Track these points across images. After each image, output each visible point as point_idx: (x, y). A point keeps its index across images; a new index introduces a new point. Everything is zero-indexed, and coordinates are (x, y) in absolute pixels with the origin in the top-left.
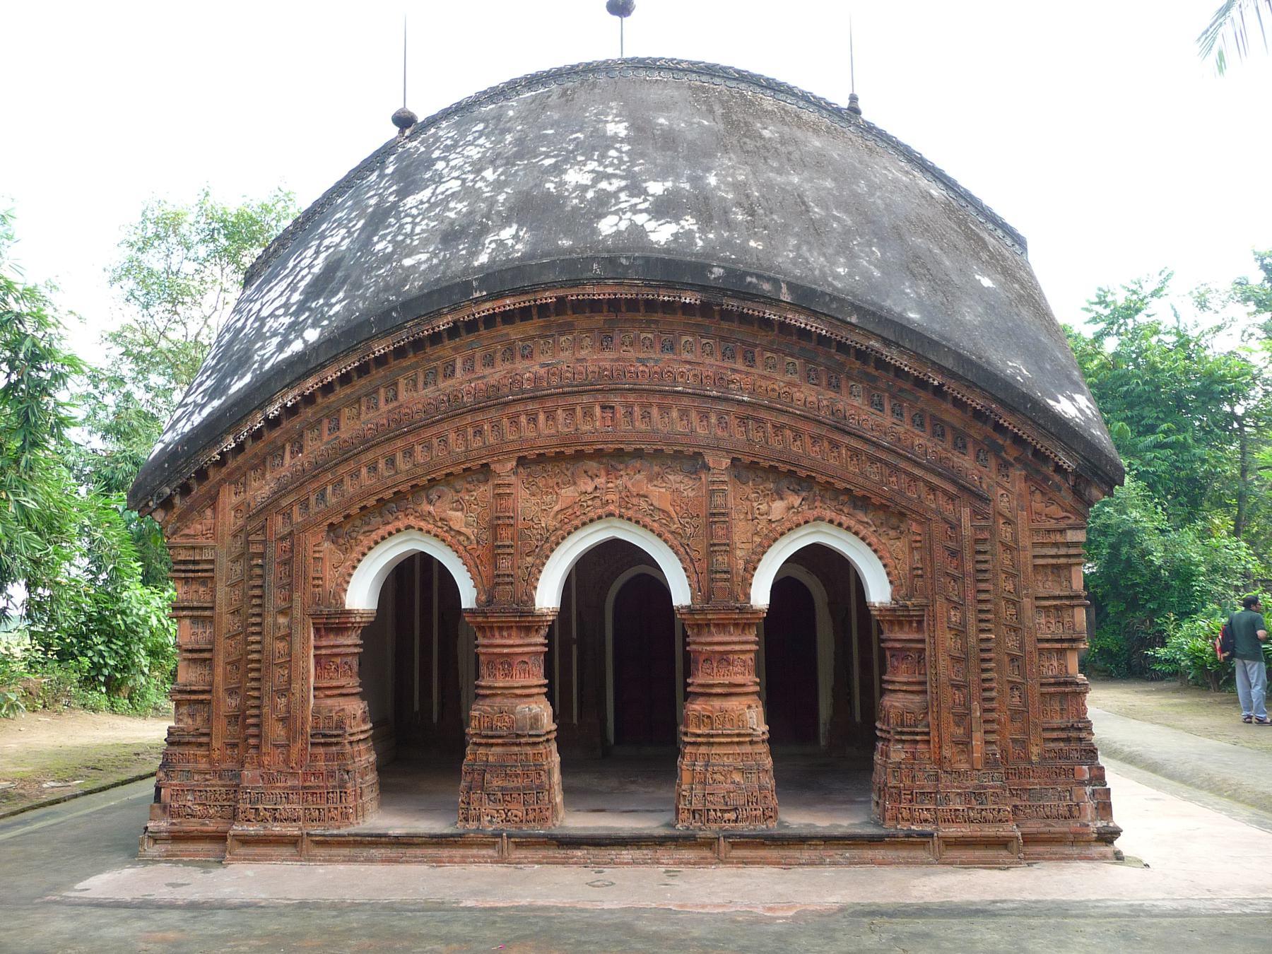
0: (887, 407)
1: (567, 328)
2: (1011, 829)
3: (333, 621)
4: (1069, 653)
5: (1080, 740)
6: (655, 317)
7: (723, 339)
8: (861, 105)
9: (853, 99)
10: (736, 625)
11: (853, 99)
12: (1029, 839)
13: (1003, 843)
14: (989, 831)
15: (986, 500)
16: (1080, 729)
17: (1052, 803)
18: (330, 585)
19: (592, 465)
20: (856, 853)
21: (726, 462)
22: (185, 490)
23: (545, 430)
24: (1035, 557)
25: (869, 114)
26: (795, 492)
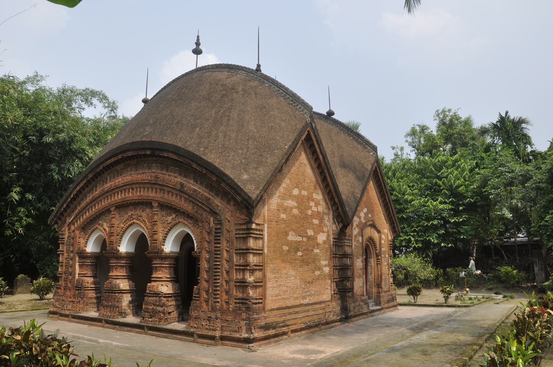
0: (199, 182)
1: (129, 165)
2: (218, 334)
3: (82, 255)
4: (246, 271)
5: (246, 303)
6: (146, 159)
7: (161, 164)
8: (262, 68)
9: (259, 66)
10: (159, 258)
11: (259, 66)
12: (223, 338)
13: (213, 338)
14: (210, 333)
15: (218, 214)
16: (246, 300)
17: (234, 327)
18: (82, 245)
19: (131, 207)
20: (129, 329)
21: (157, 204)
22: (60, 219)
23: (119, 197)
24: (236, 234)
25: (265, 71)
26: (175, 213)
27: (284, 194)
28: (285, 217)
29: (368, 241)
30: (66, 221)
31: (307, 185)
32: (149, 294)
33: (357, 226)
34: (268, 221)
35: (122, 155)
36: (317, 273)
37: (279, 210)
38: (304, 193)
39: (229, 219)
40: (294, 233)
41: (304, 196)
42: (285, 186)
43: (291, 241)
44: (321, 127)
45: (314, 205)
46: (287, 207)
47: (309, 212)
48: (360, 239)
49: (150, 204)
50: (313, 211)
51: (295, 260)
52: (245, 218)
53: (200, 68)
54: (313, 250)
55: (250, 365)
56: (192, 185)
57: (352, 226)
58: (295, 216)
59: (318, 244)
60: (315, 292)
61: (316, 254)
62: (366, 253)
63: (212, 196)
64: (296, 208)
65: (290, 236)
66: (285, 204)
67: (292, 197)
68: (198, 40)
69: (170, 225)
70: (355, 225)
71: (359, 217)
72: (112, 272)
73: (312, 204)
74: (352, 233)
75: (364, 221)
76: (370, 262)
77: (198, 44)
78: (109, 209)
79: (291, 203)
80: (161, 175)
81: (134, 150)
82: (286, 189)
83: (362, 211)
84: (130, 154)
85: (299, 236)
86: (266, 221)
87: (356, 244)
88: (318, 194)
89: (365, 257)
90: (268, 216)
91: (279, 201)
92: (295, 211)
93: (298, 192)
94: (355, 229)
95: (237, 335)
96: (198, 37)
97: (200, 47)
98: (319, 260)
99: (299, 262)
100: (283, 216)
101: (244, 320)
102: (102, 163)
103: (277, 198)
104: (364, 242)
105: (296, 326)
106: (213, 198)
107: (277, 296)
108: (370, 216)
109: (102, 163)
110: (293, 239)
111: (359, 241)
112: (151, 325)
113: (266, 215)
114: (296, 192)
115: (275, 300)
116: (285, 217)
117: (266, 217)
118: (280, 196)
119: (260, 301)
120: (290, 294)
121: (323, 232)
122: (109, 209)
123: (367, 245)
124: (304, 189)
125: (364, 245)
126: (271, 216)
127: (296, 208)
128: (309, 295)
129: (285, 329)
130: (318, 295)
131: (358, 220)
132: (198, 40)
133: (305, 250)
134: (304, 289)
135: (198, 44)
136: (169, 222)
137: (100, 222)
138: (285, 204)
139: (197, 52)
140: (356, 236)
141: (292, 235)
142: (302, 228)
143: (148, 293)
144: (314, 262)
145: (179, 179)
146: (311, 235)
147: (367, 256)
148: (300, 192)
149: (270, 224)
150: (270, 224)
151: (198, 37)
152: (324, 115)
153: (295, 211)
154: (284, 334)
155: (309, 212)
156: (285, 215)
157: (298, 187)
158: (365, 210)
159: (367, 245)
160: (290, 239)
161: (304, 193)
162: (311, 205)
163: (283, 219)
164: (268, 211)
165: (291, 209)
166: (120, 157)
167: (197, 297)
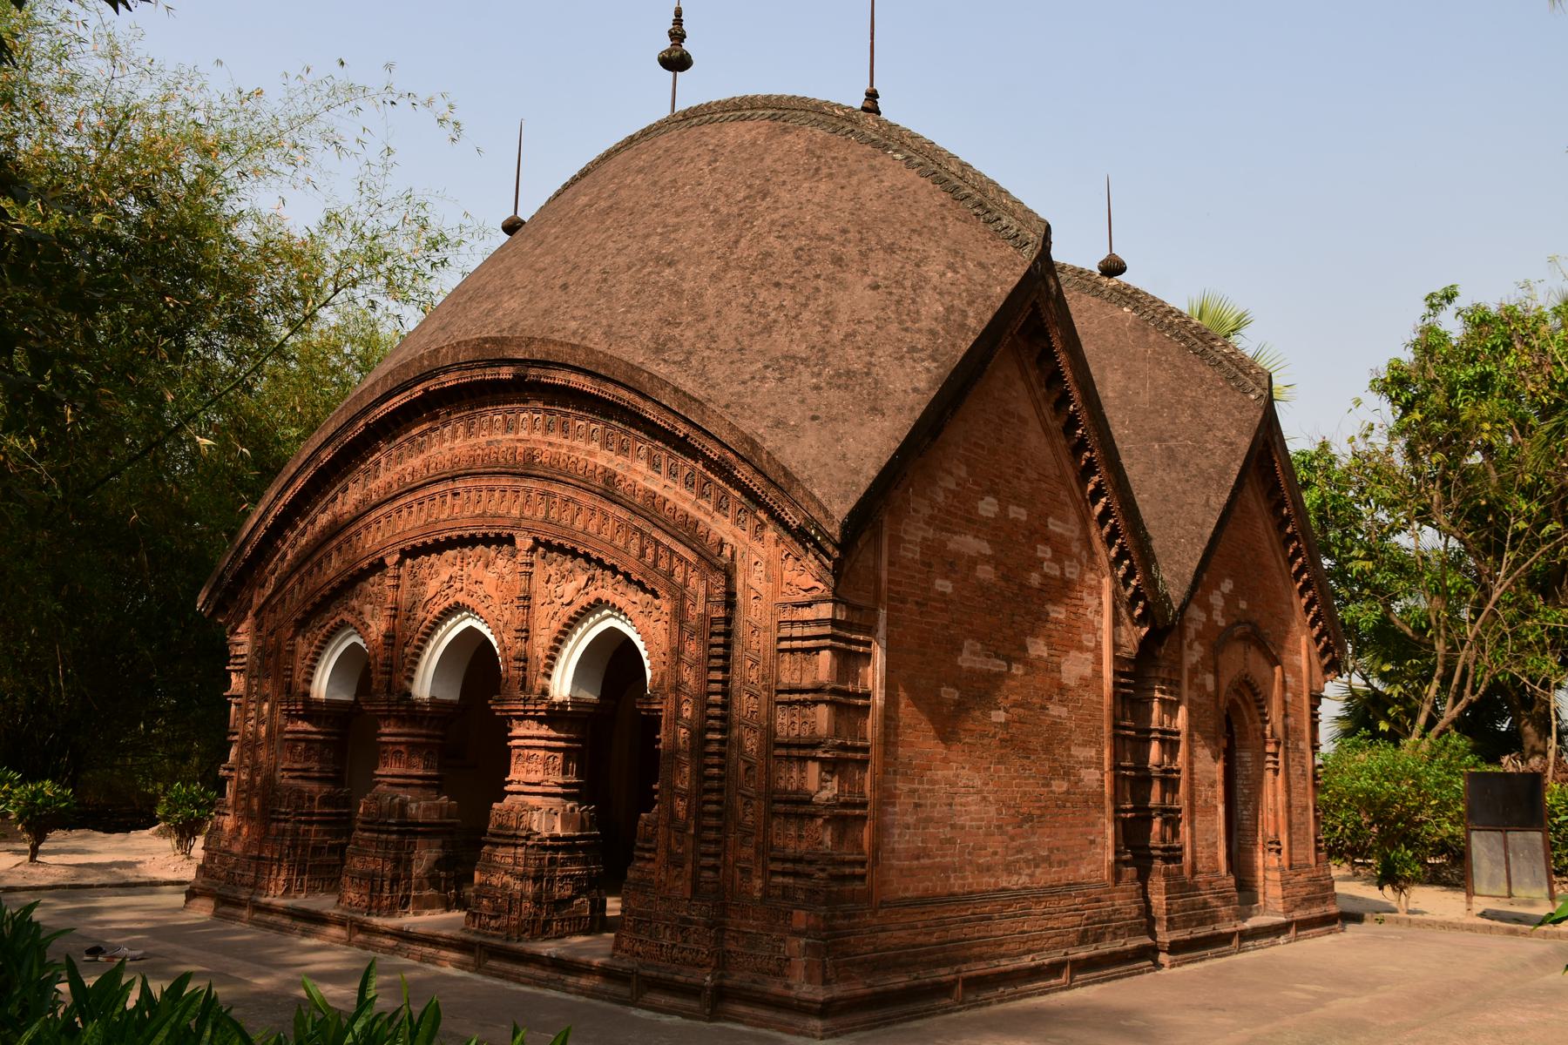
0: (663, 469)
9: (872, 95)
11: (872, 95)
27: (948, 512)
28: (949, 590)
29: (1236, 691)
30: (251, 600)
31: (1026, 487)
32: (499, 836)
33: (1199, 636)
34: (891, 599)
35: (425, 385)
36: (1059, 786)
37: (930, 565)
38: (1018, 513)
39: (758, 588)
40: (979, 646)
41: (1015, 522)
42: (953, 486)
43: (971, 671)
44: (1085, 313)
45: (1049, 554)
46: (959, 555)
47: (1035, 579)
48: (1209, 680)
49: (510, 540)
50: (1045, 576)
51: (982, 736)
52: (813, 583)
53: (684, 114)
54: (1044, 708)
55: (786, 1037)
56: (641, 472)
57: (1182, 635)
58: (984, 589)
59: (1062, 689)
60: (1051, 851)
61: (1055, 724)
62: (1230, 729)
63: (707, 513)
64: (987, 560)
65: (965, 654)
66: (951, 546)
67: (972, 522)
68: (678, 21)
69: (571, 611)
70: (1191, 633)
71: (1208, 608)
72: (386, 764)
73: (1044, 552)
74: (1181, 658)
75: (1222, 623)
76: (1243, 764)
77: (677, 35)
78: (382, 559)
79: (970, 544)
80: (544, 447)
81: (459, 366)
82: (955, 494)
83: (1218, 588)
84: (450, 380)
85: (997, 656)
86: (885, 597)
87: (1194, 695)
88: (1065, 520)
89: (1224, 743)
90: (890, 582)
91: (930, 533)
92: (985, 573)
93: (996, 509)
94: (1190, 647)
95: (776, 988)
96: (678, 13)
97: (685, 46)
98: (1066, 743)
99: (995, 743)
100: (944, 585)
101: (799, 933)
102: (365, 412)
103: (921, 524)
104: (1223, 694)
105: (982, 965)
106: (708, 520)
107: (918, 858)
108: (1243, 605)
109: (365, 412)
110: (978, 666)
111: (1204, 686)
112: (497, 942)
113: (884, 575)
114: (988, 507)
115: (910, 869)
116: (949, 590)
117: (884, 585)
118: (932, 517)
119: (858, 870)
120: (962, 853)
121: (1081, 648)
122: (382, 559)
123: (1232, 702)
124: (1017, 499)
125: (1223, 704)
126: (899, 584)
127: (987, 560)
128: (1027, 861)
129: (944, 974)
130: (1060, 863)
131: (1203, 617)
132: (678, 21)
133: (1016, 705)
134: (1012, 839)
135: (677, 35)
136: (566, 600)
137: (355, 603)
138: (951, 546)
139: (676, 62)
140: (1194, 672)
141: (974, 653)
142: (1011, 632)
143: (493, 835)
144: (1047, 749)
145: (605, 459)
146: (1040, 657)
147: (1231, 741)
148: (1004, 510)
149: (900, 610)
150: (900, 610)
151: (678, 13)
152: (1091, 273)
153: (985, 573)
154: (944, 989)
155: (1035, 579)
156: (948, 583)
157: (994, 492)
158: (1227, 586)
159: (1232, 702)
160: (965, 665)
161: (1018, 513)
162: (1040, 554)
163: (943, 594)
164: (891, 564)
165: (973, 562)
166: (418, 391)
167: (649, 850)
